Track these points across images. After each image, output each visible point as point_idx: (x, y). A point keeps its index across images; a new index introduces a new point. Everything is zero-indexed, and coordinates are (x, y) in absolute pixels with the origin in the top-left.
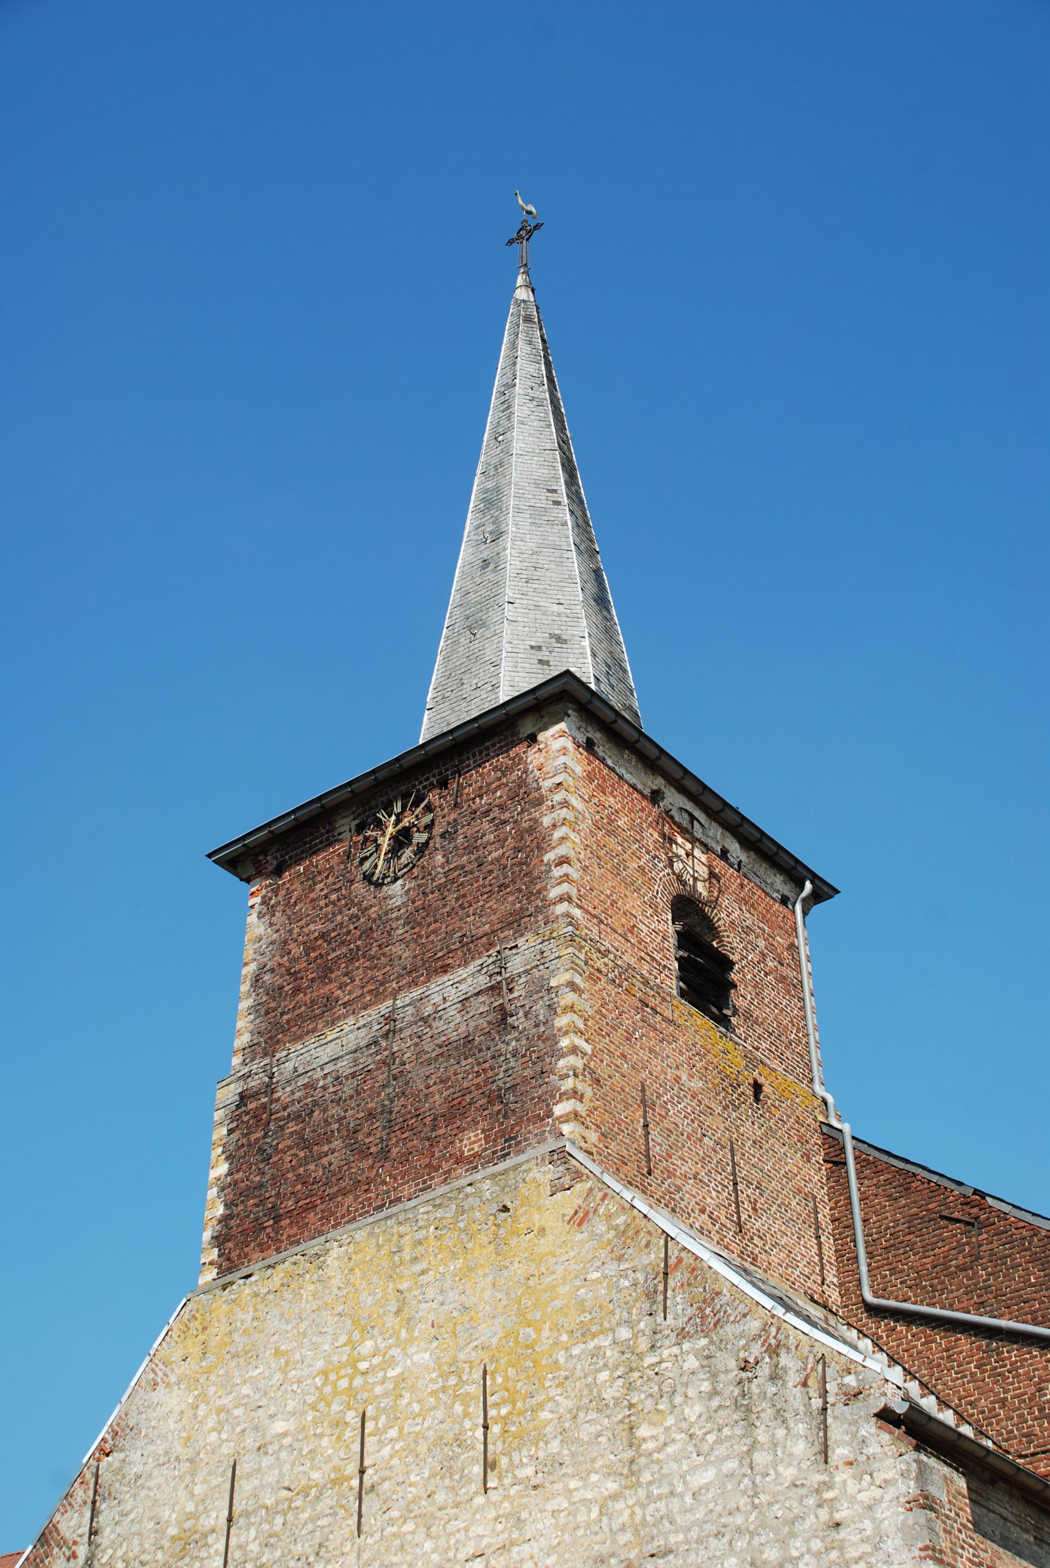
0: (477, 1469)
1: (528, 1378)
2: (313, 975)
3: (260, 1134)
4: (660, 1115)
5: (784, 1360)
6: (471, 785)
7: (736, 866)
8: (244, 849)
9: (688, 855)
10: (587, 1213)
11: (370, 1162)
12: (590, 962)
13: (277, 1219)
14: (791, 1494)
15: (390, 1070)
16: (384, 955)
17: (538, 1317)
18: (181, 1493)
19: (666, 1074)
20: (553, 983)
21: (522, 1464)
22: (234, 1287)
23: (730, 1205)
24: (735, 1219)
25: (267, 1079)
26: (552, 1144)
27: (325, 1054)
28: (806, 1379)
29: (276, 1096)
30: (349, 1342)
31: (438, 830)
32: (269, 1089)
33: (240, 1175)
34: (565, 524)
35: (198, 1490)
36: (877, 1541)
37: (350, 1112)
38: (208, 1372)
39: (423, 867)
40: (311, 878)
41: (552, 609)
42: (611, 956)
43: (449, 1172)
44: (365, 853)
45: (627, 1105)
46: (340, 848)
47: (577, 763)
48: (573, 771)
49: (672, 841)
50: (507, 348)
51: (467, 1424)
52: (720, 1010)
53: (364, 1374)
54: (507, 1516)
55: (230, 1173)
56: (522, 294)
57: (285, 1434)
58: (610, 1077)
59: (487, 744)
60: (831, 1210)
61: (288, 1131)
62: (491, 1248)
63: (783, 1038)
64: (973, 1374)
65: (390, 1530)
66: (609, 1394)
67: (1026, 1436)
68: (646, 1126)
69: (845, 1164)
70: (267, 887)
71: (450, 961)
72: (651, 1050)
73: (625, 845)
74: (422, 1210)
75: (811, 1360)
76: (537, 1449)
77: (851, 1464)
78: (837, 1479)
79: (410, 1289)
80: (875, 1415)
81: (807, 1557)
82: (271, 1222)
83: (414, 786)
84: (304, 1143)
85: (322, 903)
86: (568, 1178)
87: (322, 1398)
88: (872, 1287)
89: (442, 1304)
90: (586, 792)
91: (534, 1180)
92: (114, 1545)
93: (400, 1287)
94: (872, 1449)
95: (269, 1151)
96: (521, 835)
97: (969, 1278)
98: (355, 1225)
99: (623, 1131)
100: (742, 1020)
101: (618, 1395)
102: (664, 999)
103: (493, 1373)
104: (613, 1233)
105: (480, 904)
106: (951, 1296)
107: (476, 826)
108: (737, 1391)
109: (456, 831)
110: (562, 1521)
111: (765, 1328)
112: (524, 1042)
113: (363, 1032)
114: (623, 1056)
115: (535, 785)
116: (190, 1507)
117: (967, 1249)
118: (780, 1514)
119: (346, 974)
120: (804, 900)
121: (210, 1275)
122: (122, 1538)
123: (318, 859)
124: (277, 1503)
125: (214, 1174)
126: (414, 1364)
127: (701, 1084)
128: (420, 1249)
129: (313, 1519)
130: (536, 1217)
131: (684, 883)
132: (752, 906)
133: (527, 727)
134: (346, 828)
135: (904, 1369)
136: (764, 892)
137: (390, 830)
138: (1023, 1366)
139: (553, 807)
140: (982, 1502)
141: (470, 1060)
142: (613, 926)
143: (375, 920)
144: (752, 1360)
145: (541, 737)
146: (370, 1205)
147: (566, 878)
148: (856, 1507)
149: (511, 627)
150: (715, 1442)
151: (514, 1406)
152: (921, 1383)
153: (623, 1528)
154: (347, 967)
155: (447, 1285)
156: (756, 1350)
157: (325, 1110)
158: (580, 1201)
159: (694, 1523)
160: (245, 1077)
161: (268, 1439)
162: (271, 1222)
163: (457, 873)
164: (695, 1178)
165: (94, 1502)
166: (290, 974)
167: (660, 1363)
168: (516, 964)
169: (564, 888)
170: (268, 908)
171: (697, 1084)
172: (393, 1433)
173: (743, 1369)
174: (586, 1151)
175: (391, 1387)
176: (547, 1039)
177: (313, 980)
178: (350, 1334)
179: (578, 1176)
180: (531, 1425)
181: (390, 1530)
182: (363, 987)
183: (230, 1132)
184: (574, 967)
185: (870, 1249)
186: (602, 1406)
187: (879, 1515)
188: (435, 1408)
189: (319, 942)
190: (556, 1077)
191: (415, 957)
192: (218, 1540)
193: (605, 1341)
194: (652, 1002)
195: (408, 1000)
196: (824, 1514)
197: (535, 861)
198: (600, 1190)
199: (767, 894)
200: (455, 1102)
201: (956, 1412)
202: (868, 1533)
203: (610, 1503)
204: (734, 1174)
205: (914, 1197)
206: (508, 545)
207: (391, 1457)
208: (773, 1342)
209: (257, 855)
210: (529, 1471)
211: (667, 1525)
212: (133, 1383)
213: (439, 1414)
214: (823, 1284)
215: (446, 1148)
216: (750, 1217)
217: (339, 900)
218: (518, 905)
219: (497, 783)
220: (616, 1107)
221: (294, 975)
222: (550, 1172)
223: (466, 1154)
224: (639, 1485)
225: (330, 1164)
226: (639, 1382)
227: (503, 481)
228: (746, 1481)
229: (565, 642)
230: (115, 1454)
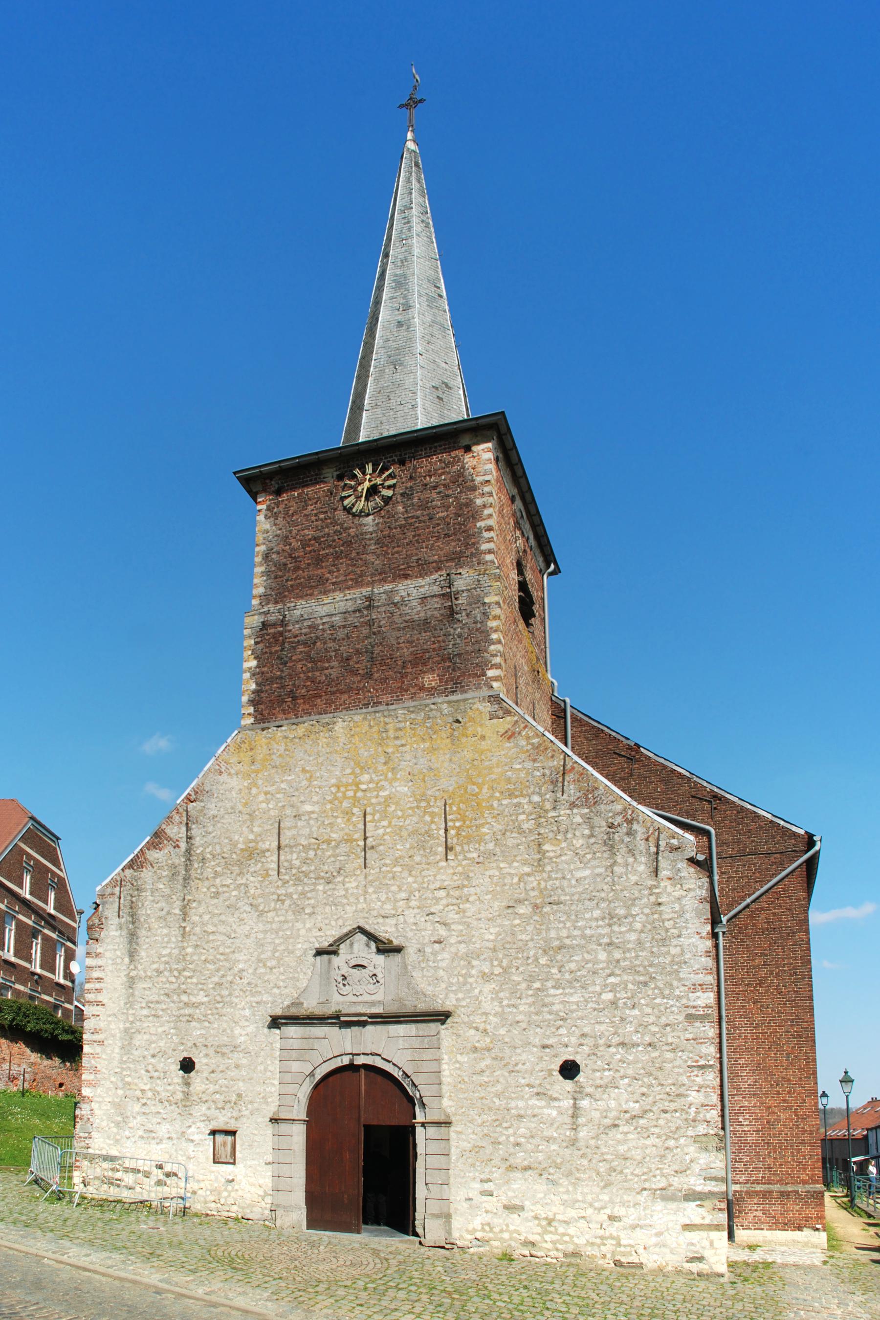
0: (441, 849)
5: (635, 826)
10: (514, 734)
13: (295, 698)
16: (361, 559)
20: (487, 600)
27: (322, 611)
28: (648, 837)
30: (353, 773)
32: (283, 623)
34: (445, 311)
36: (681, 914)
38: (257, 772)
40: (304, 502)
44: (344, 494)
46: (324, 487)
50: (404, 181)
51: (433, 826)
54: (461, 874)
55: (258, 667)
56: (411, 145)
57: (313, 812)
66: (525, 826)
70: (270, 500)
71: (410, 572)
75: (651, 829)
77: (670, 879)
78: (662, 884)
79: (393, 753)
83: (381, 459)
84: (309, 658)
85: (313, 518)
89: (416, 764)
91: (478, 709)
93: (387, 750)
96: (460, 506)
108: (605, 837)
109: (412, 494)
111: (625, 810)
112: (466, 630)
113: (350, 603)
115: (470, 478)
116: (251, 837)
119: (334, 565)
122: (205, 845)
126: (396, 791)
128: (400, 733)
133: (465, 440)
143: (353, 537)
144: (616, 824)
145: (474, 448)
146: (360, 702)
147: (490, 540)
151: (464, 823)
153: (533, 889)
156: (619, 819)
157: (325, 643)
159: (576, 893)
169: (491, 546)
170: (271, 513)
175: (382, 800)
177: (309, 564)
181: (384, 869)
183: (256, 643)
186: (521, 832)
189: (312, 542)
193: (524, 801)
196: (653, 899)
206: (416, 315)
210: (475, 855)
213: (415, 819)
218: (458, 549)
224: (543, 871)
226: (545, 824)
227: (408, 272)
228: (609, 878)
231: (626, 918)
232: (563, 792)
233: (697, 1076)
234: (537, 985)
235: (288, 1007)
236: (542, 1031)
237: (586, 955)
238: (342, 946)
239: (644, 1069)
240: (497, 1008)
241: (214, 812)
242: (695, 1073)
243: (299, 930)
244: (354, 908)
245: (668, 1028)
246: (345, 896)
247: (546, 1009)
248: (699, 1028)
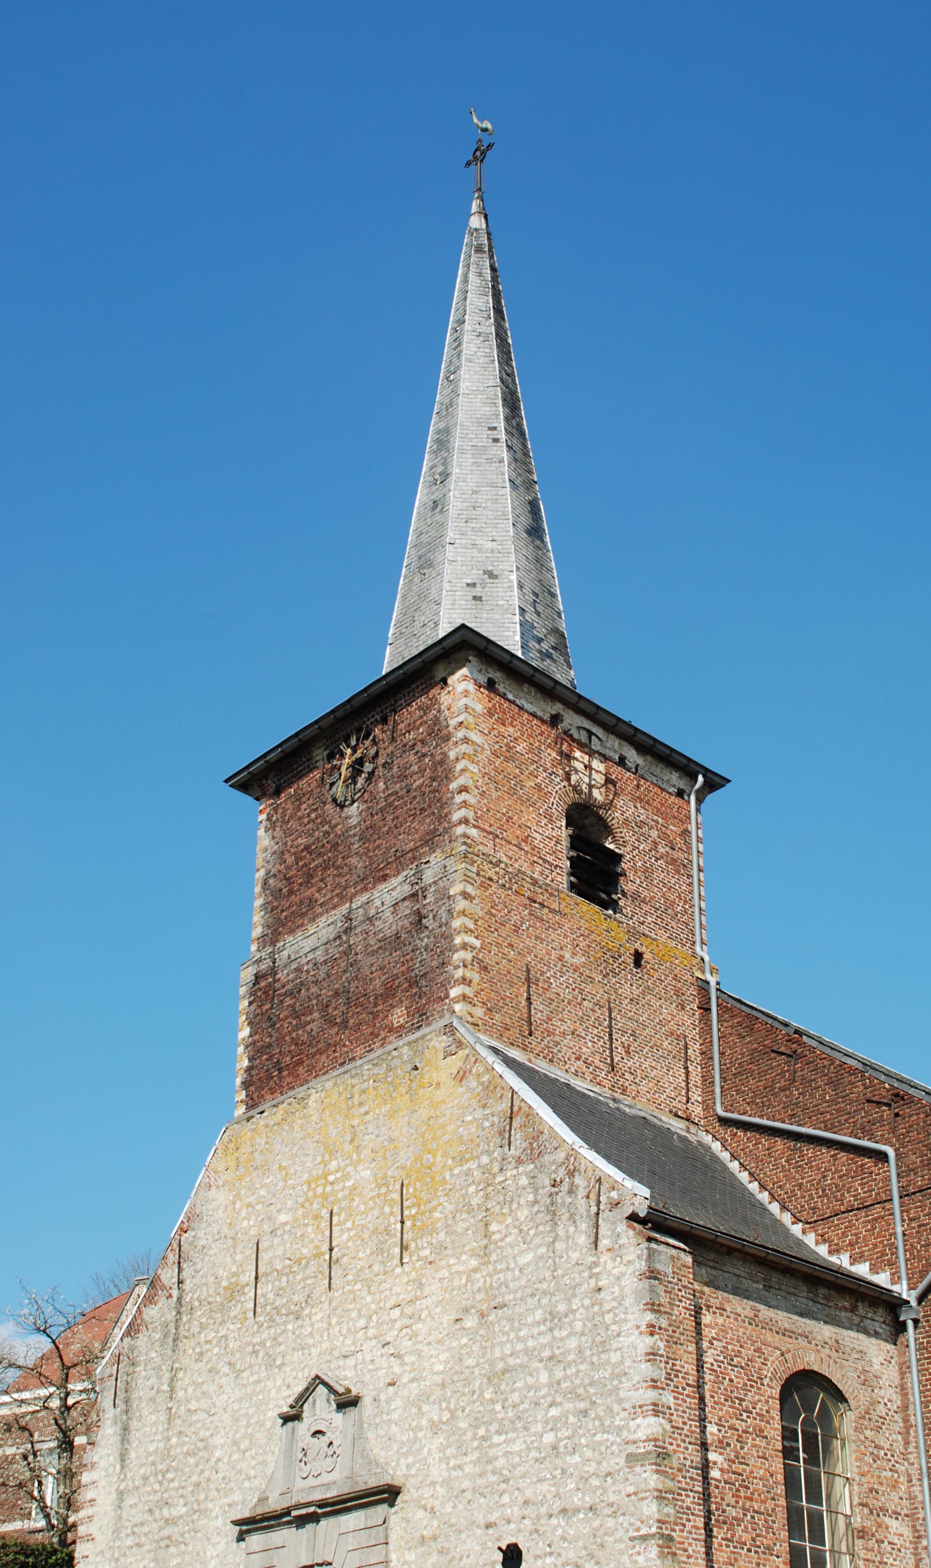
0: (397, 1250)
1: (428, 1189)
2: (301, 880)
3: (268, 1006)
4: (543, 988)
5: (578, 1180)
6: (403, 722)
7: (633, 770)
8: (250, 776)
9: (586, 767)
10: (465, 1073)
11: (336, 1029)
12: (482, 873)
13: (280, 1070)
14: (575, 1269)
15: (348, 959)
16: (346, 865)
17: (434, 1147)
18: (228, 1259)
19: (550, 955)
20: (452, 893)
21: (424, 1248)
22: (254, 1120)
23: (604, 1051)
24: (608, 1061)
25: (271, 964)
27: (308, 944)
29: (278, 976)
31: (381, 760)
32: (273, 971)
35: (238, 1257)
36: (620, 1299)
37: (324, 991)
38: (240, 1179)
39: (371, 792)
40: (298, 799)
41: (486, 547)
42: (503, 866)
43: (384, 1039)
46: (317, 774)
47: (478, 702)
48: (473, 710)
49: (569, 757)
51: (392, 1220)
52: (609, 895)
53: (332, 1184)
54: (414, 1281)
55: (251, 1036)
57: (286, 1223)
58: (497, 963)
59: (413, 686)
60: (701, 1045)
61: (285, 1004)
62: (407, 1097)
63: (670, 911)
64: (783, 1166)
65: (348, 1288)
66: (475, 1201)
67: (813, 1209)
68: (529, 999)
69: (710, 1009)
70: (270, 805)
71: (388, 871)
72: (537, 938)
73: (523, 767)
74: (366, 1067)
75: (593, 1180)
76: (432, 1238)
77: (610, 1250)
78: (602, 1260)
79: (359, 1125)
80: (627, 1218)
81: (581, 1309)
82: (276, 1073)
83: (364, 722)
85: (306, 820)
86: (454, 1046)
87: (307, 1200)
88: (722, 1103)
90: (485, 726)
91: (434, 1047)
92: (193, 1291)
94: (623, 1241)
95: (274, 1019)
97: (787, 1097)
98: (324, 1078)
99: (507, 1005)
100: (630, 901)
101: (480, 1202)
102: (552, 895)
103: (408, 1185)
104: (480, 1087)
105: (408, 824)
106: (774, 1110)
108: (549, 1201)
109: (393, 762)
110: (445, 1285)
112: (432, 939)
115: (445, 723)
116: (234, 1269)
117: (787, 1075)
118: (568, 1282)
119: (322, 880)
120: (697, 791)
121: (241, 1110)
122: (197, 1287)
123: (303, 783)
124: (284, 1268)
126: (361, 1178)
127: (583, 959)
129: (304, 1280)
130: (435, 1074)
131: (580, 792)
132: (648, 802)
134: (320, 757)
135: (740, 1163)
136: (660, 788)
137: (347, 761)
138: (815, 1160)
139: (457, 742)
140: (718, 1267)
141: (398, 953)
142: (509, 839)
143: (339, 837)
144: (558, 1180)
145: (450, 680)
146: (337, 1062)
148: (611, 1278)
149: (451, 567)
150: (534, 1235)
152: (750, 1173)
153: (479, 1290)
154: (322, 874)
155: (381, 1122)
157: (308, 989)
158: (460, 1064)
159: (520, 1288)
160: (258, 961)
161: (277, 1226)
162: (276, 1073)
163: (393, 798)
164: (573, 1033)
165: (179, 1263)
166: (286, 879)
167: (505, 1181)
168: (429, 876)
171: (579, 960)
172: (349, 1225)
173: (553, 1186)
174: (472, 1024)
176: (447, 937)
177: (301, 884)
178: (323, 1156)
179: (460, 1044)
180: (429, 1222)
181: (348, 1288)
182: (333, 891)
183: (250, 1003)
184: (467, 880)
185: (724, 1075)
187: (623, 1283)
188: (373, 1208)
189: (305, 853)
190: (452, 968)
191: (366, 867)
192: (250, 1290)
193: (473, 1165)
194: (540, 898)
195: (359, 904)
196: (592, 1282)
197: (444, 789)
198: (474, 1056)
199: (663, 790)
200: (389, 985)
201: (770, 1194)
202: (616, 1294)
203: (472, 1274)
204: (610, 1026)
205: (756, 1035)
207: (348, 1240)
208: (571, 1167)
209: (261, 780)
210: (426, 1252)
211: (504, 1288)
213: (376, 1213)
214: (688, 1102)
215: (383, 1020)
216: (623, 1058)
217: (317, 818)
219: (420, 721)
220: (501, 986)
222: (445, 1040)
223: (395, 1025)
224: (489, 1262)
225: (312, 1030)
228: (550, 1261)
229: (496, 577)
230: (189, 1232)
231: (566, 1316)
232: (509, 1145)
233: (639, 1553)
234: (482, 1432)
235: (255, 1506)
236: (486, 1501)
237: (528, 1379)
238: (306, 1406)
239: (585, 1548)
240: (444, 1473)
241: (203, 1242)
242: (637, 1549)
244: (318, 1349)
245: (609, 1479)
246: (311, 1335)
247: (490, 1467)
248: (639, 1474)
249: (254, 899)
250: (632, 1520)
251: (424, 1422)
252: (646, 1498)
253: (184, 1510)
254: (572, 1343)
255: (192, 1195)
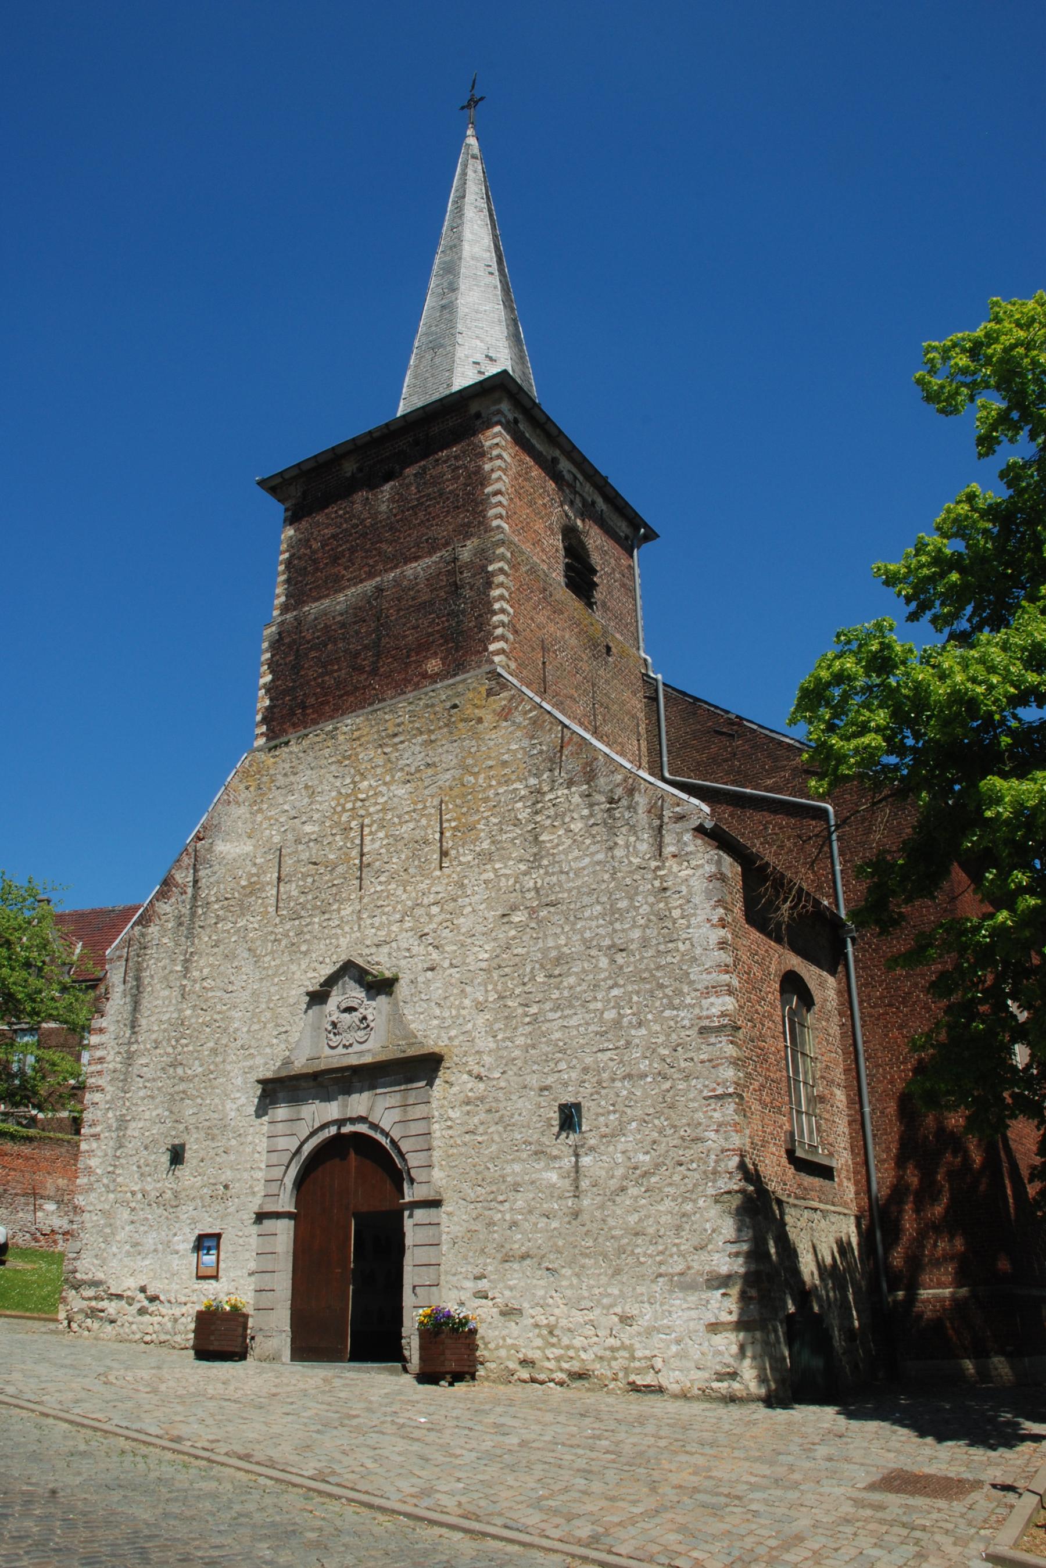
0: (436, 856)
5: (637, 797)
11: (365, 676)
13: (304, 708)
21: (464, 854)
26: (486, 668)
33: (280, 682)
45: (533, 649)
53: (362, 801)
55: (273, 681)
57: (313, 833)
68: (544, 663)
72: (548, 618)
107: (439, 469)
111: (625, 780)
114: (532, 619)
119: (349, 561)
125: (262, 681)
156: (619, 792)
165: (195, 865)
177: (327, 564)
186: (517, 823)
212: (215, 801)
215: (416, 668)
221: (315, 562)
235: (279, 1068)
242: (713, 1106)
243: (293, 973)
249: (278, 575)
250: (707, 1083)
251: (467, 1002)
252: (722, 1064)
253: (200, 1070)
254: (636, 934)
255: (210, 809)
